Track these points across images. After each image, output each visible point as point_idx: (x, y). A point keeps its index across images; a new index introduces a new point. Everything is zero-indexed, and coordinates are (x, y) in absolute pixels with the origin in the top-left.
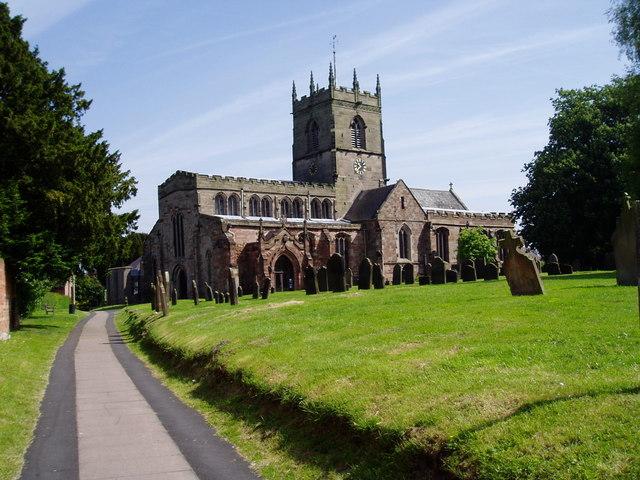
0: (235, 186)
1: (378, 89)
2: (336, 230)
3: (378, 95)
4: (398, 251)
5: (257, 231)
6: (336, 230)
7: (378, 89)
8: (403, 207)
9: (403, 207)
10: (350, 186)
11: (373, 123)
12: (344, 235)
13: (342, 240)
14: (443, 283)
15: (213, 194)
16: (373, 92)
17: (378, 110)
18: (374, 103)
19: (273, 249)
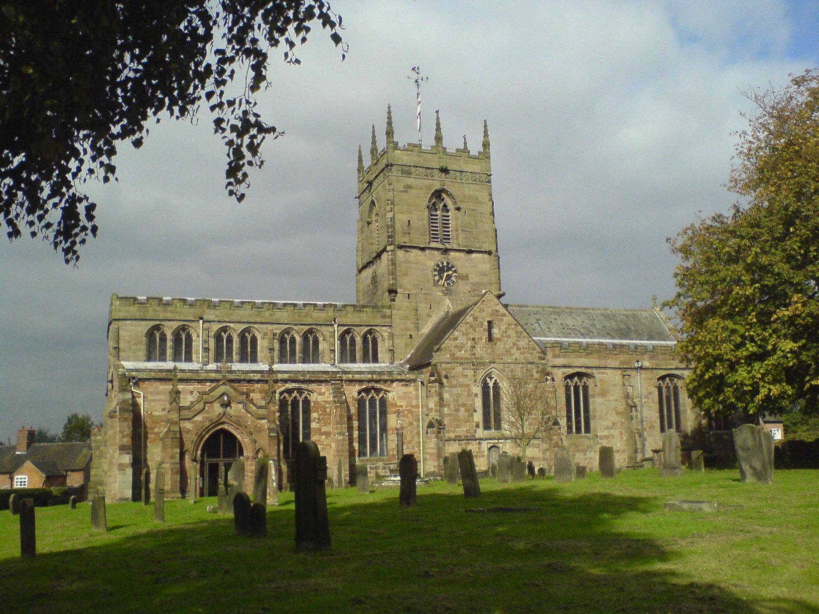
0: (246, 313)
1: (486, 145)
2: (361, 381)
3: (485, 154)
4: (478, 417)
5: (169, 387)
6: (361, 381)
7: (486, 145)
8: (490, 338)
9: (490, 338)
10: (423, 307)
11: (476, 200)
12: (378, 391)
13: (372, 401)
14: (247, 362)
15: (144, 327)
16: (475, 148)
17: (486, 179)
18: (476, 167)
19: (199, 418)
